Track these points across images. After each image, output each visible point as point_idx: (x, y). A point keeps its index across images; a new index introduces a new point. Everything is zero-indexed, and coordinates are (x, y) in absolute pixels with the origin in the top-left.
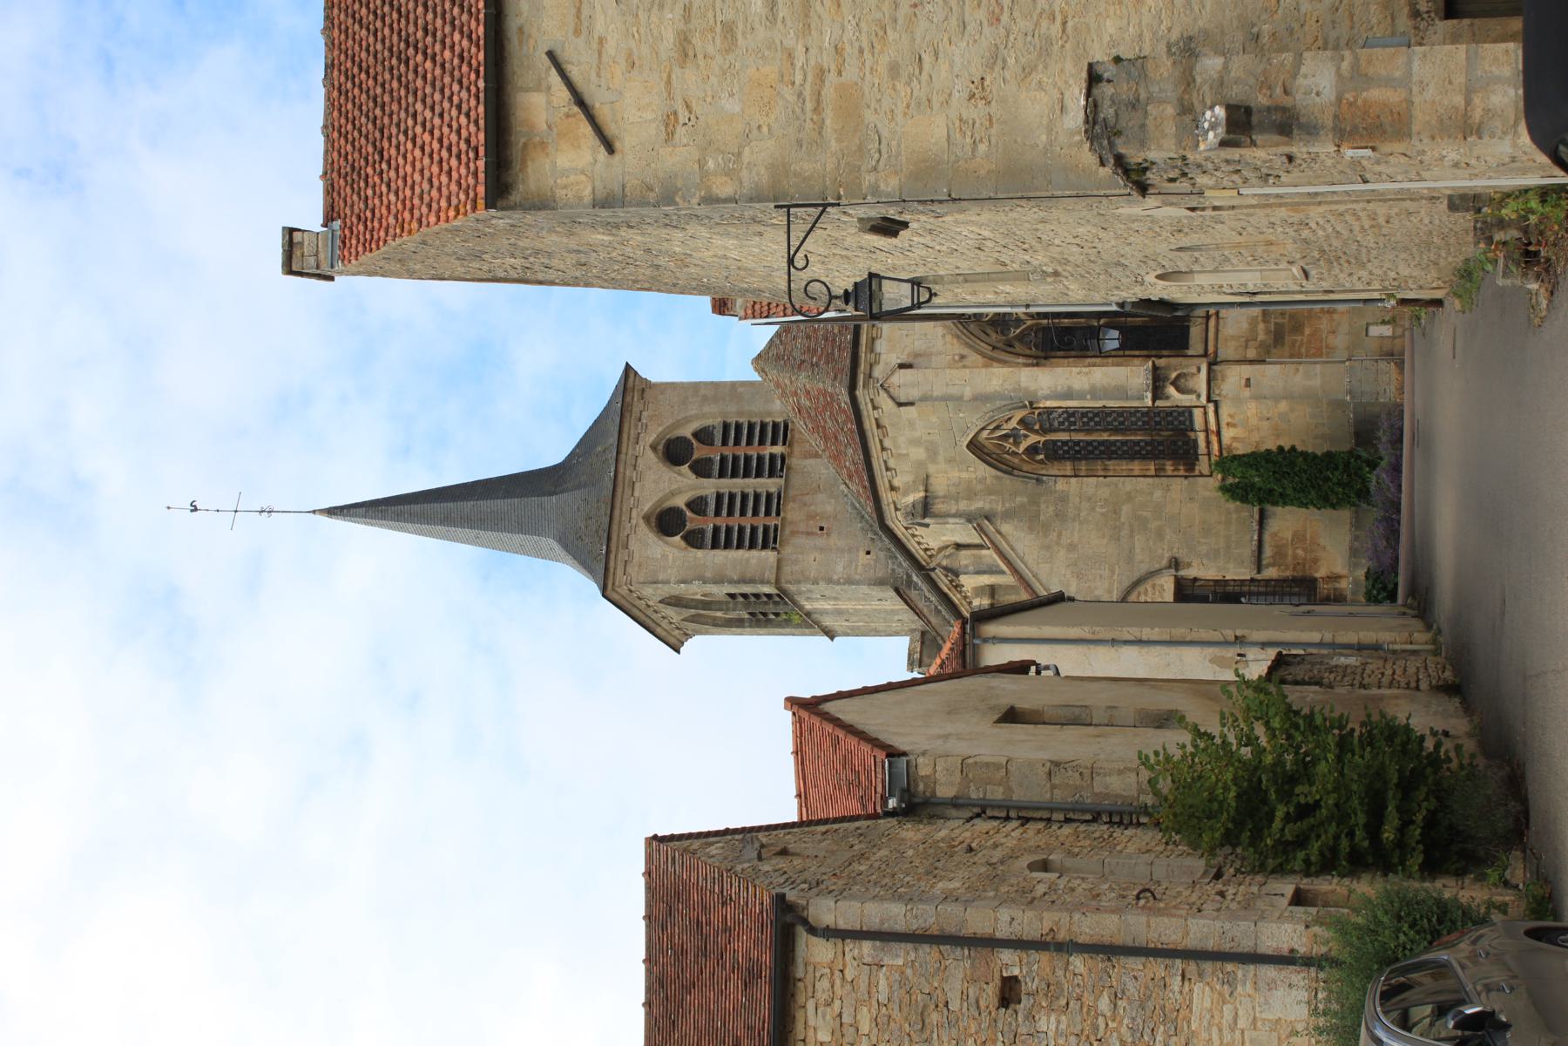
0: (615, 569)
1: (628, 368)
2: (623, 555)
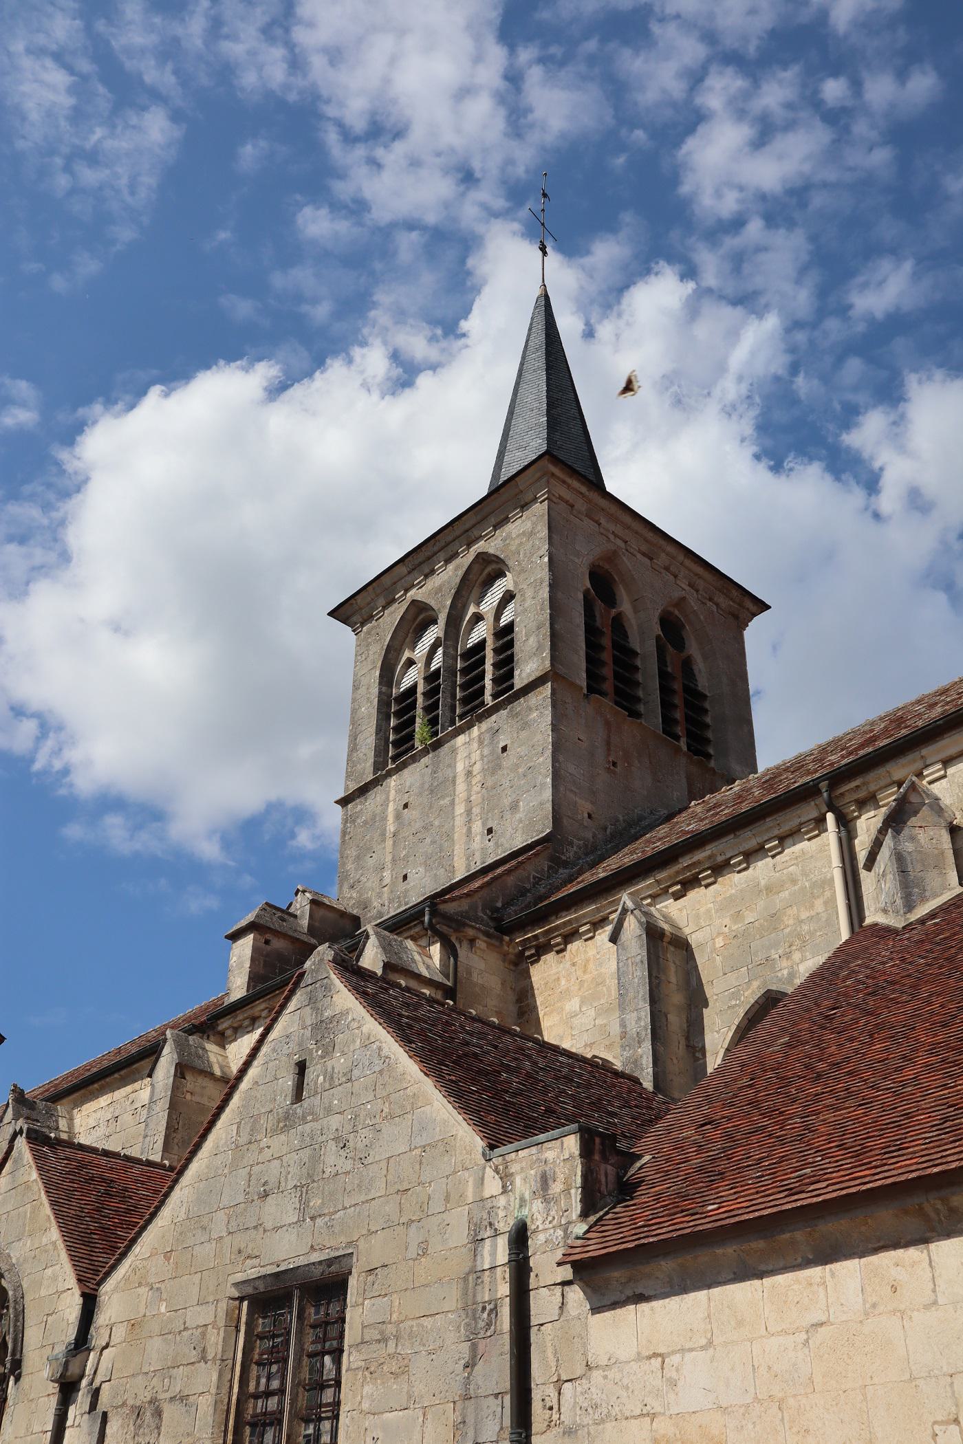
0: (569, 486)
1: (768, 607)
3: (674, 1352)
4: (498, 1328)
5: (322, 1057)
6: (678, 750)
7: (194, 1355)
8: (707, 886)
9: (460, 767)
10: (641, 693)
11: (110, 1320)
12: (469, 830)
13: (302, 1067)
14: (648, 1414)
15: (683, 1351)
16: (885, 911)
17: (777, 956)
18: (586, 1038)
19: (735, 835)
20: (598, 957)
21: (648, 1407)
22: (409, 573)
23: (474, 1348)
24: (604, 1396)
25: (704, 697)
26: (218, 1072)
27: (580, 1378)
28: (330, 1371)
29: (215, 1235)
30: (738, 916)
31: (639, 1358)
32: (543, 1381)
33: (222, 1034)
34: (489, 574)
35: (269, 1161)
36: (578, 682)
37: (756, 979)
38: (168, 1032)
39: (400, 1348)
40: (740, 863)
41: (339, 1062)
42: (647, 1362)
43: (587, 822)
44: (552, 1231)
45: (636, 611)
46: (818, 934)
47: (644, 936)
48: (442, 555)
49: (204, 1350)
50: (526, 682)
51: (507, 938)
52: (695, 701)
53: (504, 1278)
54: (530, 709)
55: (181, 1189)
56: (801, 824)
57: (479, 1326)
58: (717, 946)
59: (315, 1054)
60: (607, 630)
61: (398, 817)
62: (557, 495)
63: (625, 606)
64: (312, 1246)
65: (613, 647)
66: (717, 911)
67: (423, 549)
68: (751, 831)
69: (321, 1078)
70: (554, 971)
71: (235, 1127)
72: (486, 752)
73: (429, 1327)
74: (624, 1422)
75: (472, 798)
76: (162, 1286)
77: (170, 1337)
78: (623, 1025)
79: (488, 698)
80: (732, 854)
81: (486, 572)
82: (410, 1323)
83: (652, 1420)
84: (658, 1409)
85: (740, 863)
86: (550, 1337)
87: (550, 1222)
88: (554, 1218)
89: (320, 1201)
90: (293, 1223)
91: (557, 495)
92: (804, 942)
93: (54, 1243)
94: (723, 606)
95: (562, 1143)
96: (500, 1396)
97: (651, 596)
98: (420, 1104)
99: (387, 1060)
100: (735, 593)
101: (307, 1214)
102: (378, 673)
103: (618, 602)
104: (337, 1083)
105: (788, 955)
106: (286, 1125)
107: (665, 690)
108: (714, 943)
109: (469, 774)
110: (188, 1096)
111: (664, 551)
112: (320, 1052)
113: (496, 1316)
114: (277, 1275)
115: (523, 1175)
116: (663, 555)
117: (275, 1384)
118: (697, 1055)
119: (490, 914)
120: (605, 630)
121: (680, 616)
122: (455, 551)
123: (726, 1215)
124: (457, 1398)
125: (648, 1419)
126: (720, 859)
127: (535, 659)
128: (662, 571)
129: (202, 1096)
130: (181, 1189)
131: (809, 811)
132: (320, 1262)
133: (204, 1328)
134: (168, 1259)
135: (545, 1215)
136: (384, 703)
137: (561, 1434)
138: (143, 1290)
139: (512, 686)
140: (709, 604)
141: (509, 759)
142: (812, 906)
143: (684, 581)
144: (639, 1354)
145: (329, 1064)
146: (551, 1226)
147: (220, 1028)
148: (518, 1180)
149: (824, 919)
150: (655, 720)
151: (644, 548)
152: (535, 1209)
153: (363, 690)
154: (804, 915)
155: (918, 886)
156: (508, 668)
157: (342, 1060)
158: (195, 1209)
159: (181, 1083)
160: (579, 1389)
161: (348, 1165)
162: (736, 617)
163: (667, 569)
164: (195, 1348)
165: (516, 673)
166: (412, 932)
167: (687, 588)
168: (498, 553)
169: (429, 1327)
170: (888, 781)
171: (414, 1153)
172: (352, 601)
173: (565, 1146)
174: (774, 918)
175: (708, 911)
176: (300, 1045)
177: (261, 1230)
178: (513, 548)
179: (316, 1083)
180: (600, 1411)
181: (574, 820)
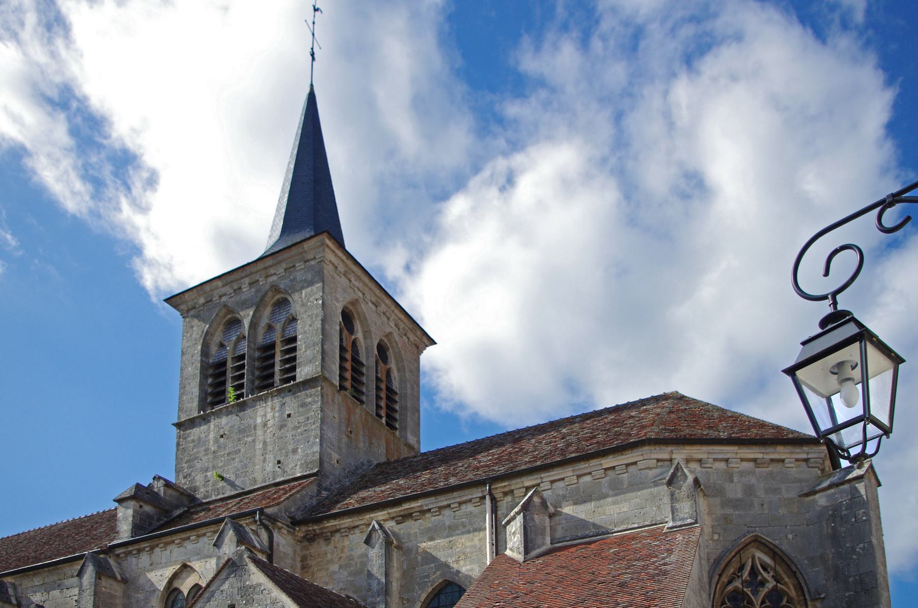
0: (336, 255)
1: (435, 343)
8: (415, 520)
9: (259, 420)
10: (364, 390)
17: (451, 561)
19: (436, 498)
22: (223, 286)
25: (396, 393)
34: (278, 300)
36: (334, 382)
37: (439, 570)
40: (436, 512)
43: (336, 465)
45: (365, 338)
47: (384, 543)
48: (247, 281)
51: (297, 529)
56: (472, 499)
60: (349, 349)
61: (216, 441)
62: (329, 260)
63: (359, 335)
66: (420, 534)
67: (235, 273)
68: (445, 497)
72: (277, 415)
79: (277, 378)
85: (436, 512)
91: (329, 260)
94: (412, 339)
97: (374, 330)
100: (419, 333)
102: (199, 347)
103: (355, 331)
110: (104, 589)
111: (384, 302)
116: (383, 305)
118: (404, 602)
119: (288, 514)
121: (388, 343)
126: (425, 508)
128: (382, 315)
129: (111, 589)
131: (476, 493)
136: (204, 367)
139: (294, 378)
140: (404, 337)
141: (291, 423)
142: (473, 540)
143: (393, 322)
147: (116, 553)
151: (373, 299)
162: (418, 348)
163: (384, 313)
165: (298, 370)
167: (394, 327)
170: (521, 486)
172: (182, 296)
181: (330, 464)
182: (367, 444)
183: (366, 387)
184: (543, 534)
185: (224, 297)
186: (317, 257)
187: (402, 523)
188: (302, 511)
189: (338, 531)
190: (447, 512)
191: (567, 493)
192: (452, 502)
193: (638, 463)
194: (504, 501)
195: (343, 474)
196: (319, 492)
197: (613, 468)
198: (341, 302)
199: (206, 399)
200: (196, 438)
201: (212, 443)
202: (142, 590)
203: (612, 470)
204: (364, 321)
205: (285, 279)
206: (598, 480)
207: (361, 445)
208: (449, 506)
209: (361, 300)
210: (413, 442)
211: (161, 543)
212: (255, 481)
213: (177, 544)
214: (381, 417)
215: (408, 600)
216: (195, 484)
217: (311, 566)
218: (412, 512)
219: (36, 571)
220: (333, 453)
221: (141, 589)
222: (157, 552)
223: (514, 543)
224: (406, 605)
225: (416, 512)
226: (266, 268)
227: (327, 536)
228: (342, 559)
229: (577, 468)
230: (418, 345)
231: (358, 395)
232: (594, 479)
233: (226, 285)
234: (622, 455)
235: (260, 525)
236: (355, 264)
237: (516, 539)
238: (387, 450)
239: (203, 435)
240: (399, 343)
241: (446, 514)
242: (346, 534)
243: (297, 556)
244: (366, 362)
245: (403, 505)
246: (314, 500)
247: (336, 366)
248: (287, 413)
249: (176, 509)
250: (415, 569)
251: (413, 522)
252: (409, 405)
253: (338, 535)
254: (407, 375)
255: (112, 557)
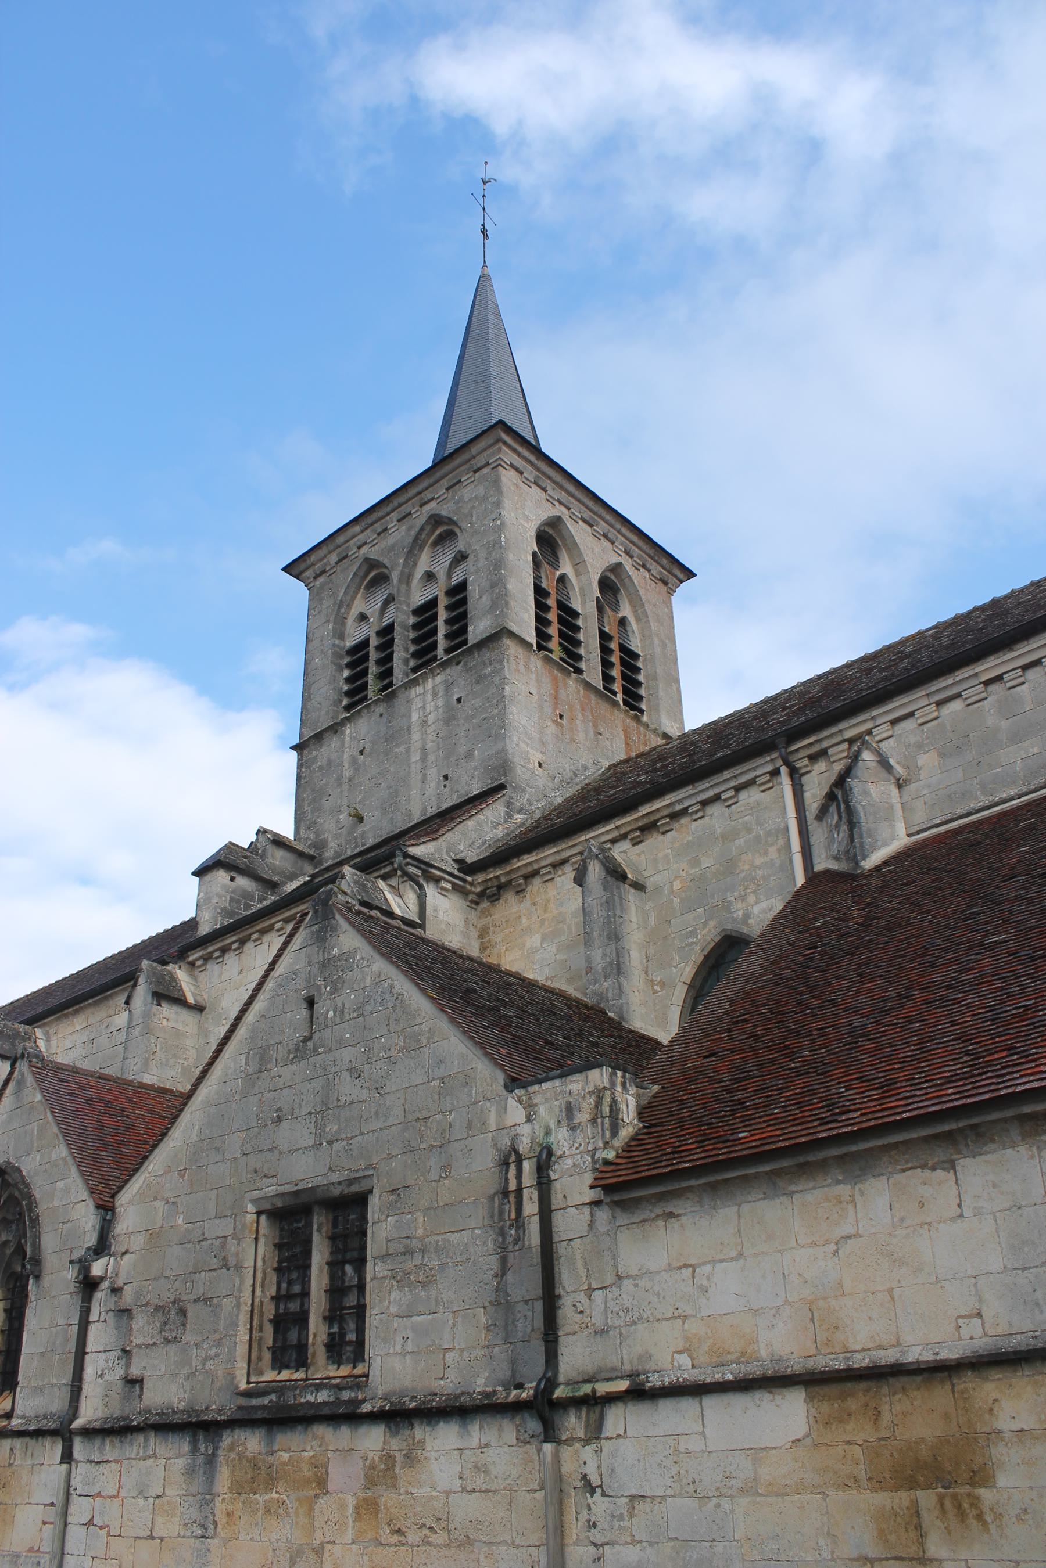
0: (519, 455)
1: (696, 575)
2: (530, 473)
3: (704, 1264)
4: (527, 1243)
5: (332, 993)
6: (615, 704)
7: (215, 1263)
8: (663, 833)
9: (415, 717)
11: (127, 1229)
12: (425, 777)
13: (310, 1002)
14: (679, 1317)
15: (713, 1262)
16: (836, 858)
17: (732, 898)
18: (547, 972)
20: (558, 897)
21: (680, 1311)
23: (504, 1260)
24: (635, 1302)
26: (191, 1000)
27: (611, 1286)
28: (352, 1278)
29: (228, 1156)
30: (695, 862)
31: (670, 1268)
32: (573, 1289)
33: (192, 964)
35: (281, 1089)
37: (712, 919)
38: (145, 963)
39: (426, 1260)
40: (697, 812)
41: (349, 998)
42: (678, 1272)
44: (579, 1156)
46: (772, 878)
48: (395, 516)
49: (225, 1259)
50: (479, 638)
52: (629, 659)
53: (531, 1199)
54: (485, 664)
55: (191, 1113)
56: (756, 777)
57: (507, 1241)
58: (675, 888)
59: (324, 990)
60: (552, 591)
61: (354, 761)
64: (330, 1168)
65: (558, 608)
69: (331, 1013)
70: (515, 909)
71: (243, 1057)
72: (440, 703)
73: (456, 1241)
74: (656, 1324)
75: (427, 747)
76: (178, 1200)
77: (189, 1246)
78: (589, 960)
79: (440, 651)
80: (689, 804)
81: (437, 532)
82: (436, 1238)
83: (684, 1323)
84: (689, 1312)
85: (697, 812)
86: (579, 1251)
87: (577, 1149)
88: (580, 1145)
89: (337, 1127)
90: (309, 1147)
92: (758, 885)
93: (64, 1159)
95: (587, 1077)
96: (530, 1302)
98: (436, 1039)
99: (400, 997)
101: (323, 1141)
104: (347, 1018)
105: (743, 898)
106: (295, 1057)
107: (605, 650)
108: (672, 886)
109: (424, 723)
110: (165, 1022)
111: (603, 519)
112: (328, 989)
113: (524, 1232)
114: (296, 1193)
115: (547, 1105)
117: (297, 1289)
118: (655, 987)
120: (550, 591)
122: (408, 512)
123: (758, 1143)
124: (487, 1304)
125: (680, 1321)
126: (678, 807)
127: (489, 616)
129: (177, 1021)
130: (191, 1113)
131: (762, 766)
132: (340, 1183)
133: (223, 1240)
134: (183, 1176)
135: (571, 1142)
137: (593, 1334)
138: (160, 1204)
139: (465, 642)
142: (766, 853)
144: (669, 1265)
145: (339, 1000)
146: (578, 1151)
148: (542, 1110)
149: (777, 865)
150: (594, 674)
152: (560, 1136)
153: (316, 643)
154: (758, 861)
155: (870, 836)
156: (460, 624)
157: (353, 997)
158: (207, 1131)
159: (158, 1010)
160: (610, 1296)
161: (364, 1094)
164: (215, 1257)
165: (470, 629)
166: (382, 872)
168: (450, 515)
169: (456, 1241)
171: (432, 1084)
173: (590, 1078)
174: (729, 866)
175: (667, 856)
176: (308, 981)
177: (276, 1152)
178: (466, 511)
179: (326, 1017)
180: (631, 1314)
182: (592, 734)
183: (585, 647)
184: (890, 819)
185: (365, 547)
186: (490, 462)
187: (641, 841)
188: (478, 848)
189: (535, 873)
190: (715, 809)
191: (923, 739)
192: (723, 789)
193: (1043, 660)
194: (814, 773)
195: (550, 784)
196: (509, 816)
197: (999, 678)
198: (532, 521)
199: (341, 701)
200: (325, 762)
201: (346, 765)
202: (225, 1019)
203: (999, 683)
204: (573, 548)
205: (448, 502)
206: (976, 706)
207: (581, 736)
208: (717, 798)
209: (566, 518)
210: (672, 731)
211: (253, 933)
212: (409, 813)
213: (278, 930)
214: (615, 693)
215: (662, 984)
216: (322, 837)
217: (496, 943)
218: (656, 818)
219: (77, 1007)
220: (531, 751)
221: (224, 1017)
222: (249, 949)
223: (839, 843)
224: (660, 994)
225: (663, 818)
226: (419, 493)
227: (519, 885)
228: (546, 923)
229: (933, 689)
230: (666, 579)
231: (572, 658)
232: (968, 705)
233: (367, 528)
234: (1013, 650)
235: (402, 876)
236: (550, 466)
237: (841, 835)
238: (627, 744)
239: (334, 756)
240: (633, 578)
241: (716, 814)
242: (550, 877)
243: (472, 928)
244: (582, 607)
245: (640, 809)
246: (501, 829)
247: (529, 614)
248: (455, 698)
249: (292, 881)
250: (670, 922)
251: (661, 837)
252: (660, 671)
253: (537, 881)
254: (652, 624)
255: (183, 967)
